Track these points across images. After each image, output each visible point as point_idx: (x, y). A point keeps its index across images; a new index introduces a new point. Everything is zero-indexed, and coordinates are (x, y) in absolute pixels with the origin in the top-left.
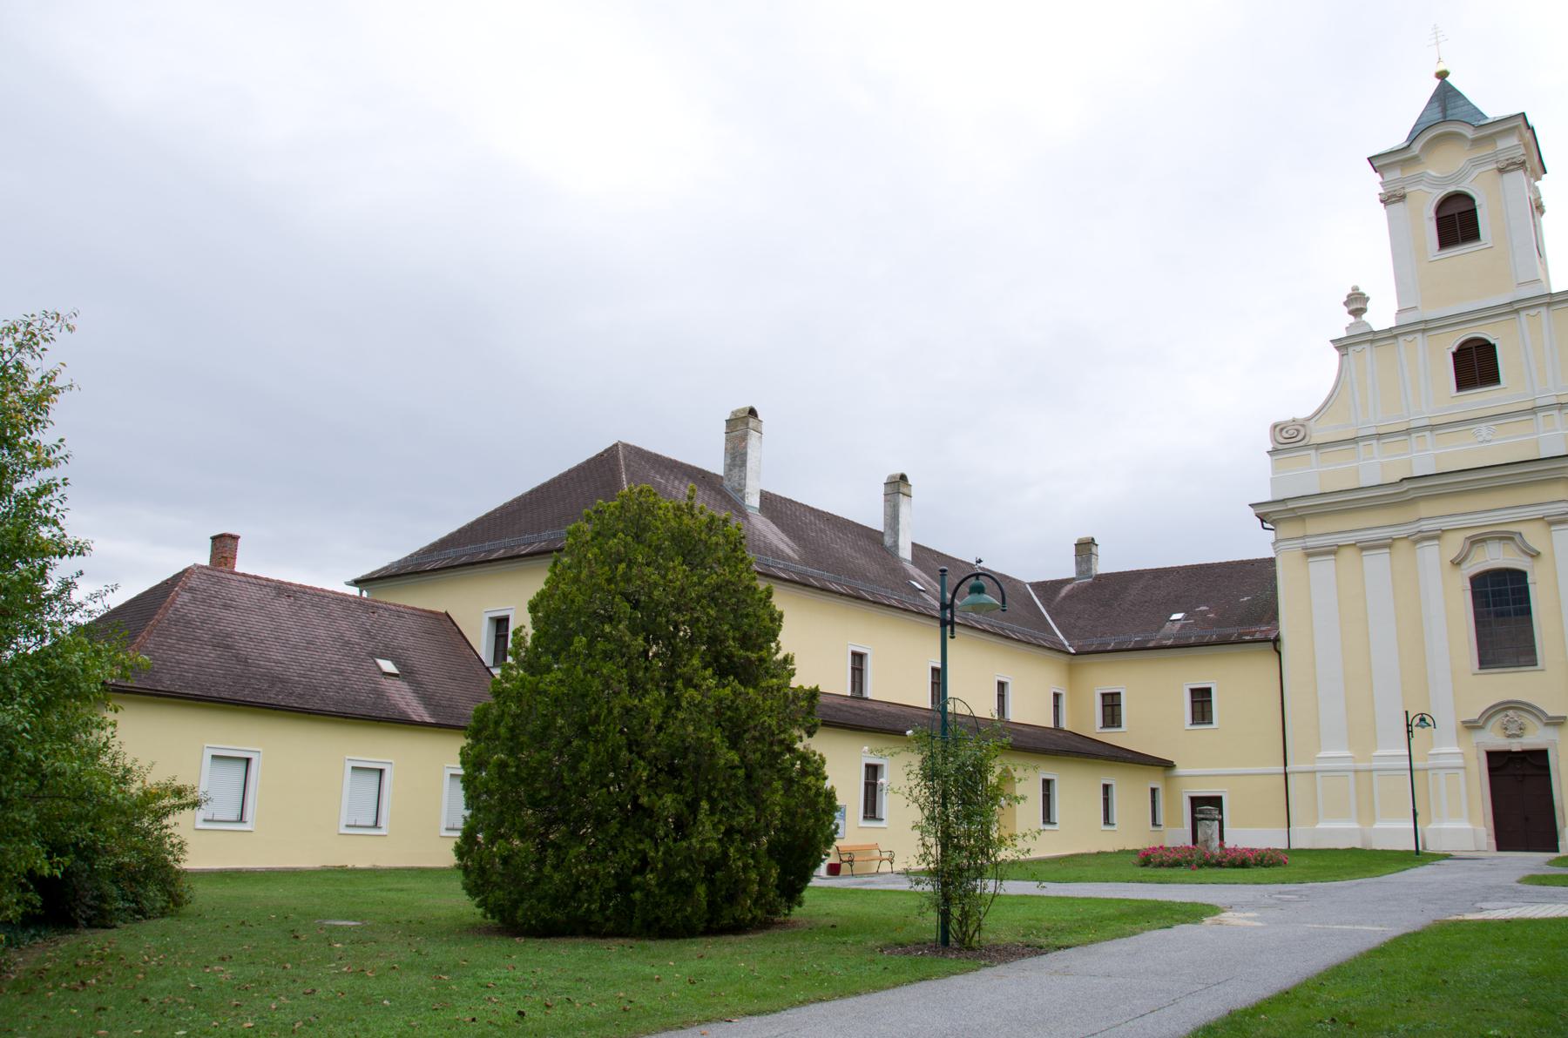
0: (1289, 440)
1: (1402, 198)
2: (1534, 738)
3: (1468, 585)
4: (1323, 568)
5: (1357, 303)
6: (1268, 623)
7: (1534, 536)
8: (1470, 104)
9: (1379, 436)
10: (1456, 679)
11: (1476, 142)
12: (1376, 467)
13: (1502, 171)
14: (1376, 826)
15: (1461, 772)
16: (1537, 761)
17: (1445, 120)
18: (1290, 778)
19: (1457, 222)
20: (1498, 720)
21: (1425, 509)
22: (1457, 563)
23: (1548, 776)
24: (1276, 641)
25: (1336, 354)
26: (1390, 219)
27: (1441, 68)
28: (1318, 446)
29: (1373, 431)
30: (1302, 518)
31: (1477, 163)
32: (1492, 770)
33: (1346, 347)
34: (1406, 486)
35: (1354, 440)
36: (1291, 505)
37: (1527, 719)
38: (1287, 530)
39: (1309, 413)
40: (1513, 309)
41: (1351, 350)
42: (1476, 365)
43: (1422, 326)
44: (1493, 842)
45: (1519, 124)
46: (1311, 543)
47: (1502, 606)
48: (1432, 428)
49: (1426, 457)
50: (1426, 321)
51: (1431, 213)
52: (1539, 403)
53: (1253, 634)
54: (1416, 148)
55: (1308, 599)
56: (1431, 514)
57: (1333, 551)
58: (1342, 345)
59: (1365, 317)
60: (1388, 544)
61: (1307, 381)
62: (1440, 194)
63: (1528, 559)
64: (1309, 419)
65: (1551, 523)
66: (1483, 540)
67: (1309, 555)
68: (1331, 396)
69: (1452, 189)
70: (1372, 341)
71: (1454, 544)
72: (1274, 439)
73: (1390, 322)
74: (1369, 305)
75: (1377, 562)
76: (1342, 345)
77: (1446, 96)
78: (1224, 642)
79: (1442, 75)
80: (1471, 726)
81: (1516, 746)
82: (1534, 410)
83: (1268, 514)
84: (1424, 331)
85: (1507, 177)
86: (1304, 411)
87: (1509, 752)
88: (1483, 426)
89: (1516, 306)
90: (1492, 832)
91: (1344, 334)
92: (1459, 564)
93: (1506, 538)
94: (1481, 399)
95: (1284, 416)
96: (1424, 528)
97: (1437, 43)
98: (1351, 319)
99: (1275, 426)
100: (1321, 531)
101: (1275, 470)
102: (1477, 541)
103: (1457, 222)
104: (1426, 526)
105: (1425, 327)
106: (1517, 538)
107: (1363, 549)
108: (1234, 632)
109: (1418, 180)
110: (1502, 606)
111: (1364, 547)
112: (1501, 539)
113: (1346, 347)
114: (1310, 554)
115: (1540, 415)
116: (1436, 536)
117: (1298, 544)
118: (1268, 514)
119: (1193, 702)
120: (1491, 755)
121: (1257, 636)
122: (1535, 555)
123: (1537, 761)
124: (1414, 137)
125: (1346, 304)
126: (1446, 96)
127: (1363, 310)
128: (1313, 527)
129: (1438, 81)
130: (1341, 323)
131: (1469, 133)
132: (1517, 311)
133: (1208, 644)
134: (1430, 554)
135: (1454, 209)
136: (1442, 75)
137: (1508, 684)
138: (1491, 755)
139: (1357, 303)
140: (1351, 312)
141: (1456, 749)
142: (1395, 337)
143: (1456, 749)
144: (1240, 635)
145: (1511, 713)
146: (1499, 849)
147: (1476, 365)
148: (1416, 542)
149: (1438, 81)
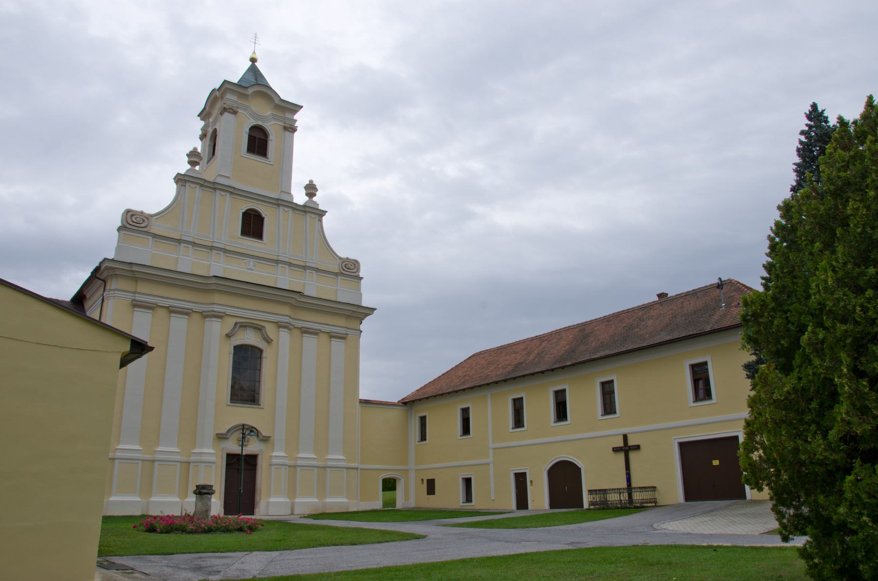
0: (133, 223)
2: (253, 447)
3: (232, 351)
7: (270, 330)
12: (187, 262)
14: (153, 499)
16: (251, 461)
21: (217, 298)
22: (228, 336)
28: (155, 236)
29: (191, 239)
31: (275, 118)
32: (229, 465)
35: (179, 241)
36: (134, 268)
39: (153, 212)
42: (252, 224)
43: (202, 182)
46: (138, 297)
50: (205, 180)
52: (281, 258)
56: (219, 302)
57: (151, 307)
58: (180, 179)
59: (314, 199)
66: (245, 326)
67: (135, 306)
69: (260, 123)
76: (180, 179)
79: (253, 60)
80: (221, 437)
82: (277, 262)
85: (287, 132)
86: (151, 208)
88: (252, 262)
89: (307, 209)
93: (259, 329)
94: (250, 244)
96: (215, 309)
98: (189, 167)
99: (128, 211)
102: (244, 326)
104: (217, 308)
107: (171, 312)
109: (246, 108)
115: (280, 265)
116: (219, 316)
117: (130, 296)
119: (625, 548)
122: (269, 341)
123: (251, 461)
125: (188, 155)
127: (315, 195)
128: (142, 287)
134: (217, 328)
135: (258, 135)
136: (253, 60)
137: (245, 414)
147: (252, 224)
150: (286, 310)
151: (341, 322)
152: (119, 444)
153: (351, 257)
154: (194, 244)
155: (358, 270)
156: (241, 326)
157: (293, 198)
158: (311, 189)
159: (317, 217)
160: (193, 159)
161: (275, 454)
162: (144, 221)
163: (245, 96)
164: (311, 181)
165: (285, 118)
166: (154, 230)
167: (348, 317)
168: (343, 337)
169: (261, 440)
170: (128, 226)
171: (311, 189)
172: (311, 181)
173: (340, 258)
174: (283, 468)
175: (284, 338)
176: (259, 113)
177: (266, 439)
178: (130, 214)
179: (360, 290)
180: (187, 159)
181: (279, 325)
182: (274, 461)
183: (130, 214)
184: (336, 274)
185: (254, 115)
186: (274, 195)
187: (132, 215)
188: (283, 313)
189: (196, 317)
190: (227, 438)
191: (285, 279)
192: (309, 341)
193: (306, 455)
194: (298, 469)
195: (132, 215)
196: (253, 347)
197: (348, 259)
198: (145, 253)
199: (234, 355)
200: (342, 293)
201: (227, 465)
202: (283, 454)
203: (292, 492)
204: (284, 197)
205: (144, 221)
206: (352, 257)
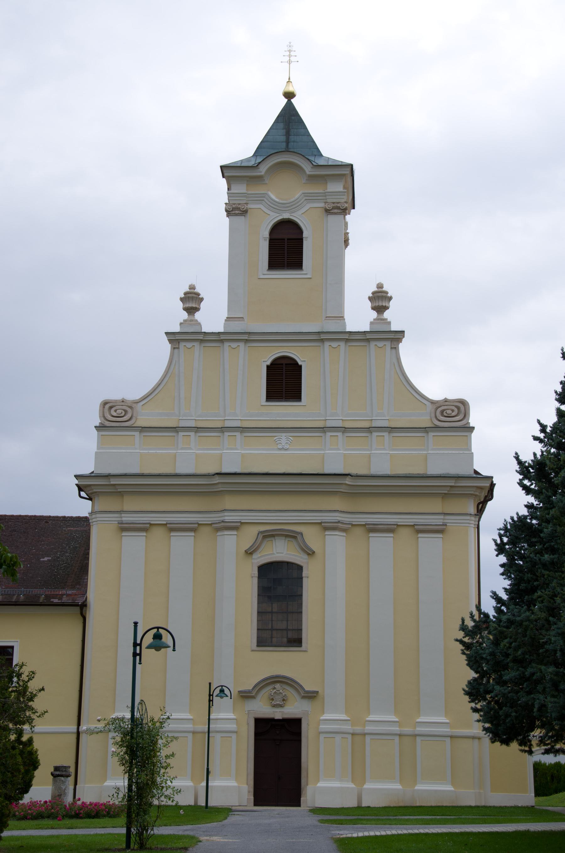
0: (116, 418)
1: (244, 213)
2: (291, 710)
4: (134, 543)
5: (192, 301)
6: (73, 587)
7: (311, 536)
8: (309, 135)
9: (197, 429)
10: (239, 658)
11: (312, 178)
12: (190, 457)
13: (328, 211)
15: (234, 736)
17: (287, 150)
18: (83, 737)
19: (286, 248)
20: (267, 691)
21: (230, 502)
22: (249, 553)
23: (300, 741)
24: (83, 607)
25: (168, 346)
26: (232, 230)
27: (291, 89)
28: (143, 429)
29: (193, 424)
30: (121, 494)
31: (310, 198)
32: (258, 735)
33: (178, 341)
34: (217, 480)
35: (175, 429)
36: (113, 481)
37: (290, 692)
38: (103, 503)
39: (137, 397)
40: (320, 338)
41: (182, 344)
42: (284, 380)
44: (252, 798)
45: (345, 172)
46: (127, 518)
47: (280, 593)
48: (243, 430)
49: (236, 455)
50: (249, 333)
51: (267, 234)
52: (329, 424)
53: (60, 597)
54: (263, 169)
55: (123, 576)
56: (234, 507)
57: (145, 528)
58: (174, 339)
59: (387, 314)
60: (193, 528)
61: (139, 366)
62: (275, 217)
63: (306, 556)
64: (137, 402)
65: (326, 529)
66: (273, 536)
67: (123, 529)
68: (158, 385)
69: (286, 216)
70: (201, 341)
71: (249, 536)
72: (103, 416)
73: (219, 327)
74: (203, 305)
75: (182, 544)
76: (174, 339)
77: (289, 121)
78: (32, 603)
79: (289, 95)
80: (246, 696)
81: (278, 714)
82: (323, 429)
83: (87, 486)
84: (246, 341)
85: (331, 218)
86: (133, 394)
87: (272, 720)
88: (283, 437)
89: (323, 337)
90: (252, 790)
91: (177, 329)
92: (251, 554)
93: (292, 536)
94: (284, 411)
95: (115, 395)
96: (227, 519)
97: (290, 62)
99: (105, 403)
100: (136, 508)
101: (101, 444)
102: (268, 536)
103: (286, 248)
104: (229, 517)
105: (248, 338)
106: (299, 537)
107: (172, 530)
108: (42, 593)
109: (261, 198)
110: (280, 593)
111: (172, 528)
112: (287, 536)
113: (178, 341)
114: (124, 528)
116: (235, 527)
117: (115, 517)
118: (87, 486)
120: (258, 721)
121: (65, 599)
122: (310, 553)
124: (256, 154)
126: (289, 121)
127: (386, 308)
128: (130, 504)
129: (286, 100)
130: (176, 317)
131: (308, 169)
132: (322, 340)
133: (16, 604)
134: (230, 544)
136: (289, 95)
137: (280, 662)
138: (258, 721)
139: (192, 301)
140: (185, 309)
141: (232, 716)
142: (222, 341)
143: (232, 716)
144: (48, 597)
145: (278, 686)
146: (255, 805)
147: (284, 380)
148: (218, 530)
149: (286, 100)
150: (336, 503)
151: (436, 505)
152: (369, 714)
153: (451, 397)
154: (344, 430)
155: (466, 415)
156: (265, 537)
157: (344, 325)
158: (380, 300)
159: (388, 344)
160: (187, 305)
161: (326, 716)
162: (126, 412)
163: (258, 180)
164: (192, 287)
165: (325, 194)
166: (141, 422)
167: (445, 496)
168: (440, 530)
169: (303, 697)
170: (107, 424)
171: (380, 300)
172: (192, 287)
173: (433, 402)
174: (338, 738)
175: (336, 547)
176: (286, 198)
177: (311, 696)
178: (107, 406)
179: (469, 449)
180: (369, 304)
181: (326, 527)
182: (323, 727)
183: (107, 406)
184: (425, 430)
185: (275, 206)
186: (314, 328)
187: (111, 408)
188: (334, 507)
189: (359, 532)
190: (253, 697)
191: (335, 456)
192: (381, 544)
193: (381, 717)
194: (419, 739)
195: (111, 408)
196: (288, 563)
197: (446, 400)
198: (134, 456)
199: (260, 577)
200: (437, 459)
201: (256, 734)
202: (344, 717)
203: (358, 774)
204: (332, 326)
205: (126, 412)
206: (452, 396)
